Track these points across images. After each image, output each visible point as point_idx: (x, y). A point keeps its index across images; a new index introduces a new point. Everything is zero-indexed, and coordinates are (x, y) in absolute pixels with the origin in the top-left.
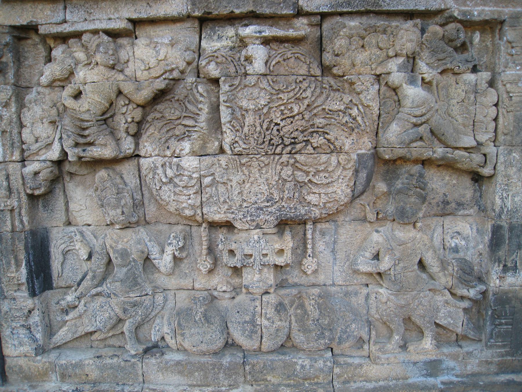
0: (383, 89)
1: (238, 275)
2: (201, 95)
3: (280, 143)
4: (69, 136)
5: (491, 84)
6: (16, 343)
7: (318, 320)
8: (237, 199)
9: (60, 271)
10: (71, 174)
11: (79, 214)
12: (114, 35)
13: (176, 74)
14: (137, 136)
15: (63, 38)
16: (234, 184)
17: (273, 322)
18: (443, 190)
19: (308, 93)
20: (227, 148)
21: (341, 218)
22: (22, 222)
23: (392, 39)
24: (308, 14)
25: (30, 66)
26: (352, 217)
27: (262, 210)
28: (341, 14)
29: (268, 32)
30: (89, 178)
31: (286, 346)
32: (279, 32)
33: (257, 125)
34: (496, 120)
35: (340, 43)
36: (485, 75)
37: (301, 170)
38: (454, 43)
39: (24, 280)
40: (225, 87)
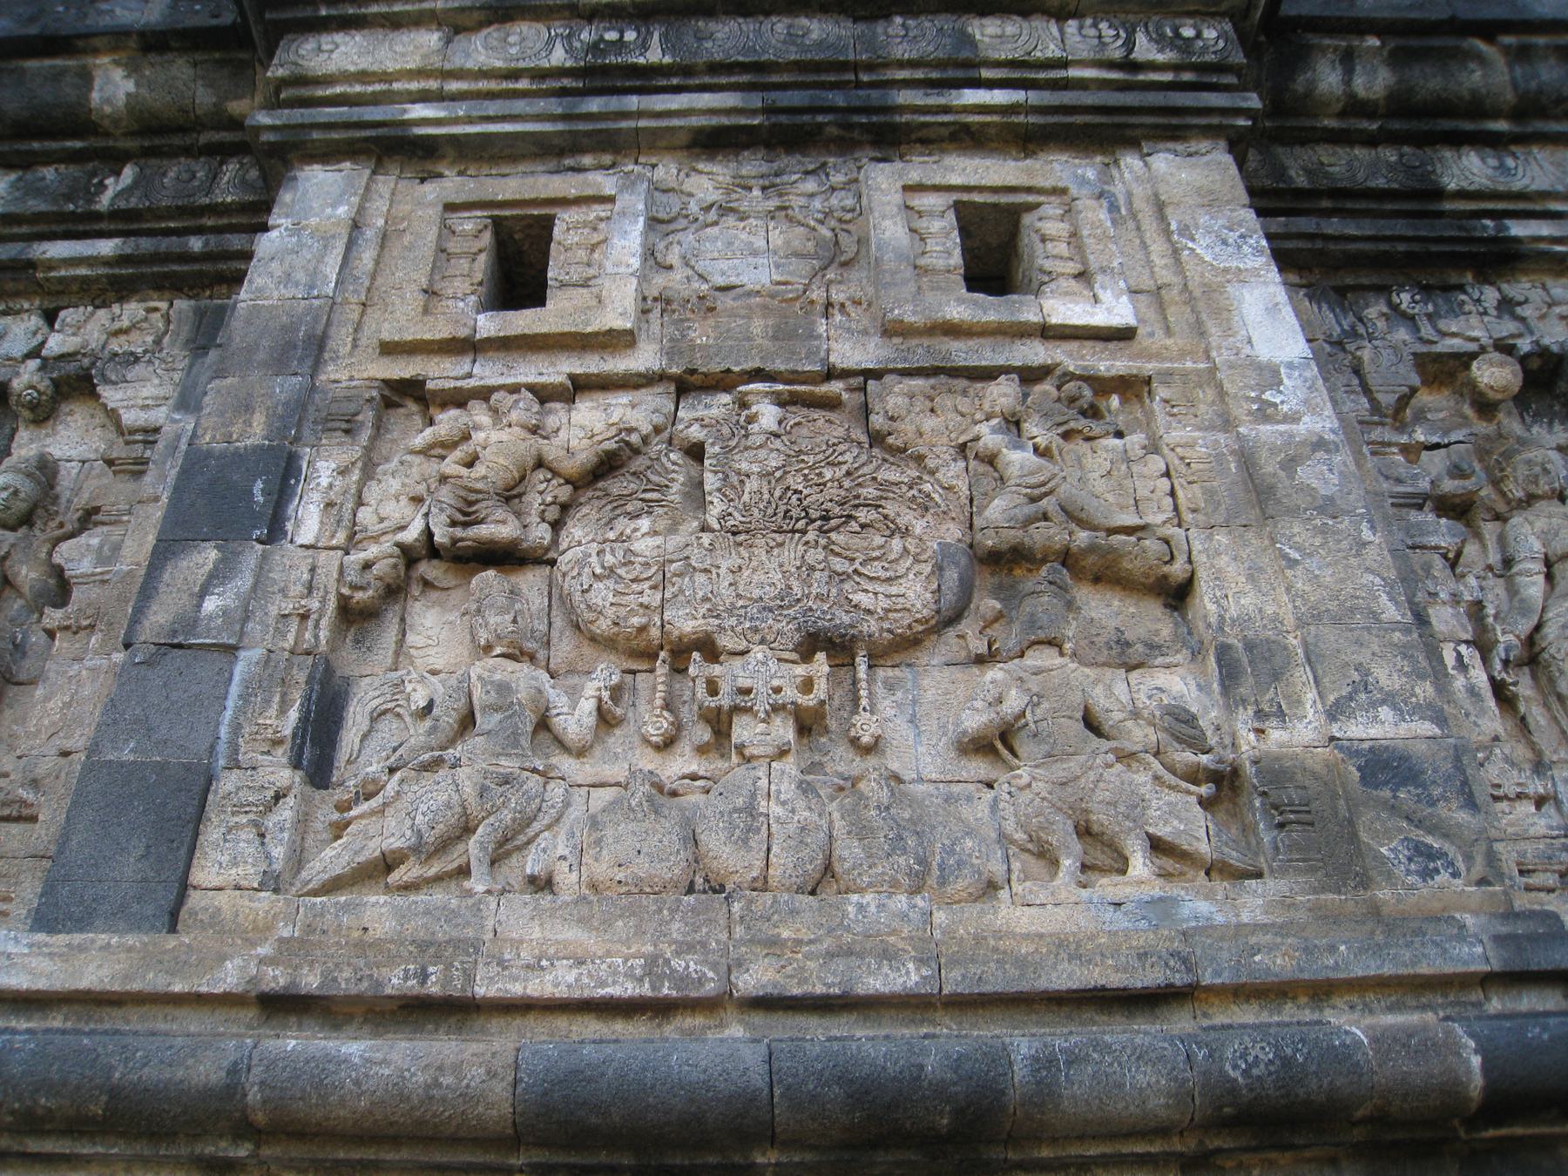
0: (973, 464)
1: (722, 756)
2: (674, 464)
4: (442, 510)
5: (1153, 448)
6: (225, 859)
7: (887, 808)
9: (356, 748)
10: (427, 584)
11: (421, 652)
12: (544, 395)
13: (634, 438)
14: (557, 526)
16: (723, 571)
17: (793, 811)
18: (1113, 623)
19: (848, 457)
21: (922, 657)
22: (316, 637)
23: (977, 402)
25: (394, 441)
26: (944, 659)
27: (771, 611)
30: (455, 596)
31: (824, 878)
33: (765, 491)
34: (1173, 494)
37: (838, 555)
38: (1078, 404)
39: (288, 732)
40: (712, 450)
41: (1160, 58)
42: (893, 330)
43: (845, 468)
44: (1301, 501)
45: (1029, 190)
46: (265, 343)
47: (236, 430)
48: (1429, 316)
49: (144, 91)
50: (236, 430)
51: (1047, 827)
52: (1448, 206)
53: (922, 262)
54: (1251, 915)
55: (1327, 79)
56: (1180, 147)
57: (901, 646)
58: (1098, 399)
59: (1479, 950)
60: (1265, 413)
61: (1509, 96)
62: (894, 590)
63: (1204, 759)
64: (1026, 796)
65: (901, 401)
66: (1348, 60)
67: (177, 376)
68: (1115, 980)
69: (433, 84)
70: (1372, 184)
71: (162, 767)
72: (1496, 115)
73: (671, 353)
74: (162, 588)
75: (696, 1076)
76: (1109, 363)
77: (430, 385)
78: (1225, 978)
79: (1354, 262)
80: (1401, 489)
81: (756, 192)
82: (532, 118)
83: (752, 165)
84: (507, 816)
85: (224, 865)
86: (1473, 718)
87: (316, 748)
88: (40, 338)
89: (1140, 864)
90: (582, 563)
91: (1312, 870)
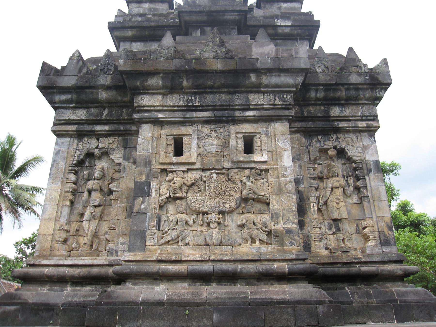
3: (220, 194)
5: (267, 182)
8: (209, 205)
10: (170, 202)
12: (184, 172)
13: (197, 180)
14: (187, 193)
15: (172, 172)
20: (207, 195)
21: (234, 213)
24: (226, 168)
28: (233, 168)
29: (217, 171)
34: (269, 189)
35: (232, 174)
36: (265, 180)
40: (207, 182)
41: (279, 103)
42: (233, 162)
44: (286, 191)
45: (255, 133)
47: (141, 178)
48: (323, 141)
49: (108, 97)
50: (141, 178)
51: (247, 238)
52: (331, 119)
53: (237, 148)
54: (268, 250)
55: (313, 94)
56: (280, 122)
57: (231, 212)
58: (262, 172)
60: (284, 176)
61: (345, 97)
63: (267, 229)
64: (245, 234)
65: (233, 174)
66: (317, 91)
67: (122, 153)
68: (252, 258)
69: (161, 108)
70: (318, 115)
71: (140, 230)
72: (342, 100)
73: (201, 165)
76: (263, 167)
77: (167, 170)
78: (264, 259)
79: (313, 131)
81: (214, 132)
82: (178, 116)
83: (213, 126)
84: (183, 236)
85: (150, 242)
87: (158, 227)
88: (97, 144)
89: (257, 243)
90: (190, 200)
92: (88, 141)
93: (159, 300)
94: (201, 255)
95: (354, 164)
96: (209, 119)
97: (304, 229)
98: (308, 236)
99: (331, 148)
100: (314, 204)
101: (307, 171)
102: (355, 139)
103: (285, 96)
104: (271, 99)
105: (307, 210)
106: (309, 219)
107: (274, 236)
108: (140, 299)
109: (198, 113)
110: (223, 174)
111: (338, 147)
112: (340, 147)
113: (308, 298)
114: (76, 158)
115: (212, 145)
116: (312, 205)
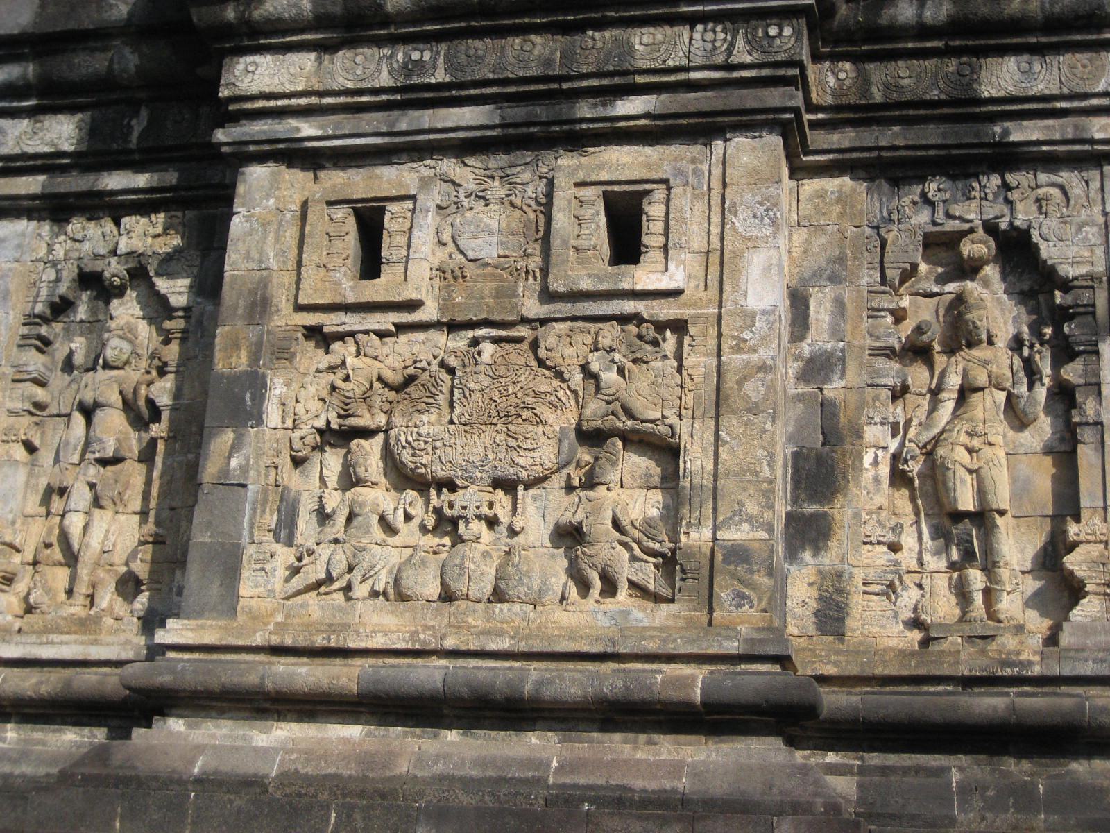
12: (382, 335)
15: (341, 337)
32: (503, 333)
41: (748, 59)
43: (519, 385)
44: (741, 404)
46: (242, 303)
47: (234, 360)
54: (651, 622)
59: (736, 644)
62: (536, 455)
67: (195, 272)
71: (223, 545)
73: (442, 309)
74: (212, 454)
75: (418, 682)
76: (666, 310)
77: (326, 330)
80: (878, 344)
81: (497, 183)
83: (497, 161)
86: (871, 495)
91: (691, 601)
92: (83, 229)
93: (255, 775)
94: (414, 634)
95: (1058, 294)
96: (478, 134)
97: (826, 548)
98: (840, 575)
99: (972, 230)
100: (880, 452)
101: (866, 323)
102: (1077, 189)
103: (773, 31)
104: (718, 44)
105: (845, 478)
106: (849, 512)
107: (683, 571)
108: (196, 770)
109: (443, 112)
110: (519, 340)
111: (1004, 225)
112: (1011, 224)
113: (754, 788)
114: (44, 292)
115: (489, 231)
116: (868, 459)
